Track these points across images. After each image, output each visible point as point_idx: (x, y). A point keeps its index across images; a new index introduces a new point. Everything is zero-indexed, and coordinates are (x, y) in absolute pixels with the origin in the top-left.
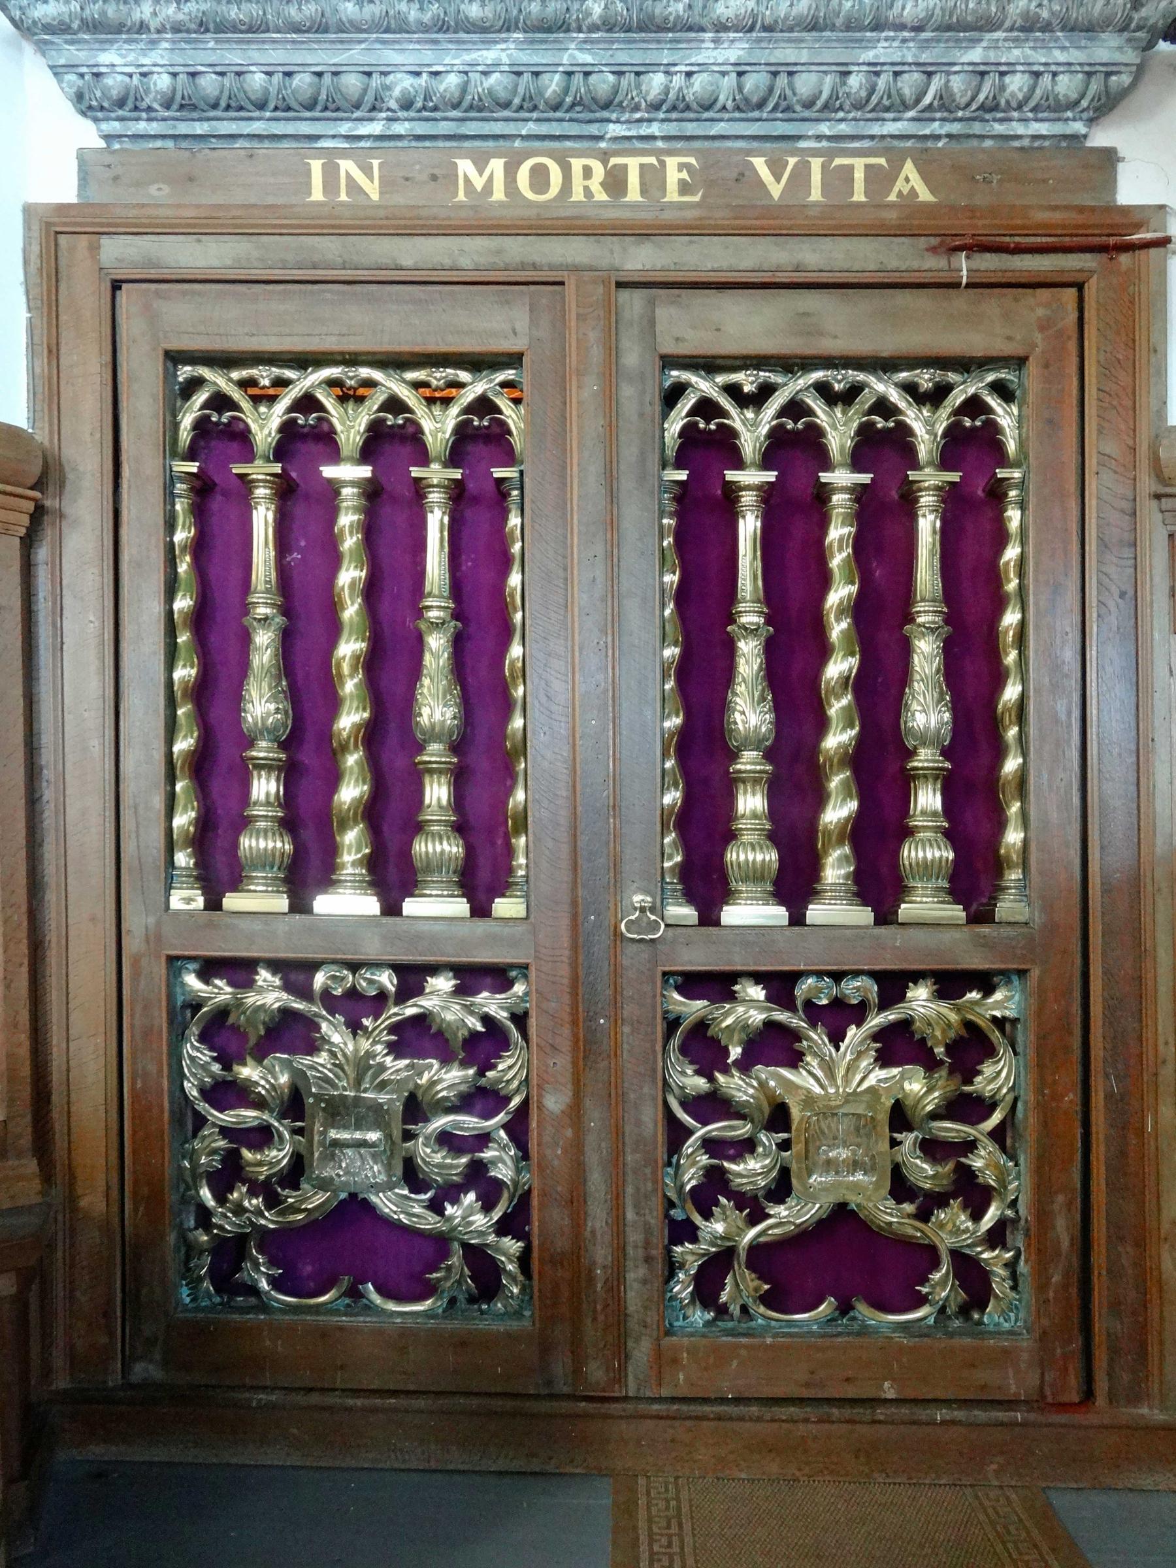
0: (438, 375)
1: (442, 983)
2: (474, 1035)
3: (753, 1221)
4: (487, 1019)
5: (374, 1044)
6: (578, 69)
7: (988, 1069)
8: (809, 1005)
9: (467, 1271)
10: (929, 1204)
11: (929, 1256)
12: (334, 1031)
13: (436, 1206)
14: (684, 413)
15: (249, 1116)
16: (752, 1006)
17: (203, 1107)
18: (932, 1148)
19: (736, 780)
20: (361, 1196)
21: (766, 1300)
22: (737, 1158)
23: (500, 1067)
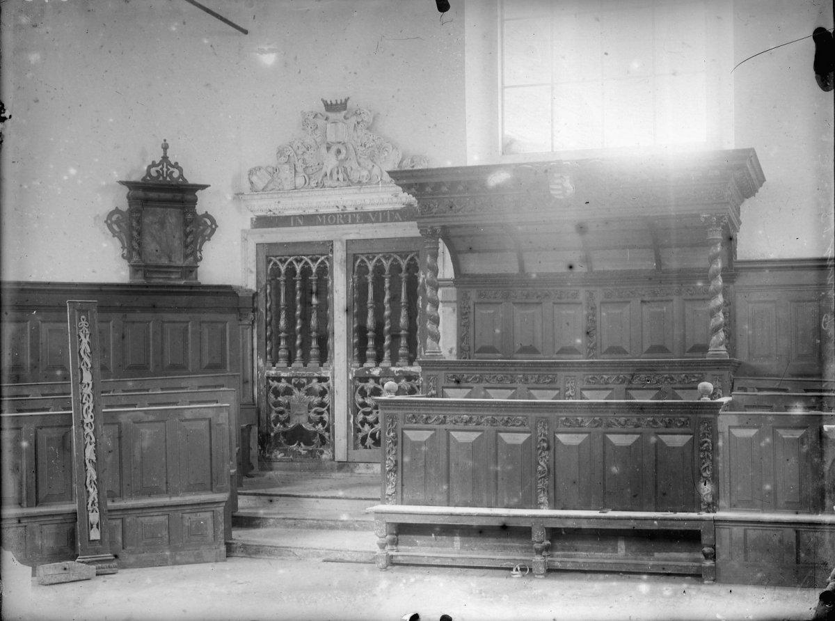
1: (315, 381)
4: (323, 388)
5: (302, 394)
7: (360, 397)
12: (296, 391)
17: (273, 407)
21: (373, 444)
22: (368, 415)
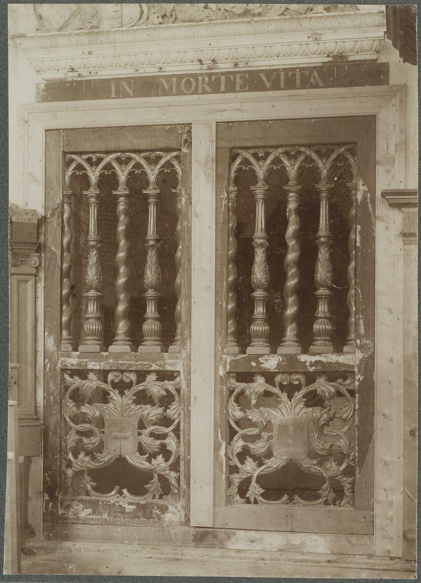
2: (163, 397)
3: (260, 464)
4: (167, 391)
6: (376, 38)
10: (322, 460)
12: (114, 395)
13: (149, 460)
14: (71, 170)
15: (254, 431)
16: (93, 383)
17: (72, 424)
18: (154, 435)
23: (172, 408)
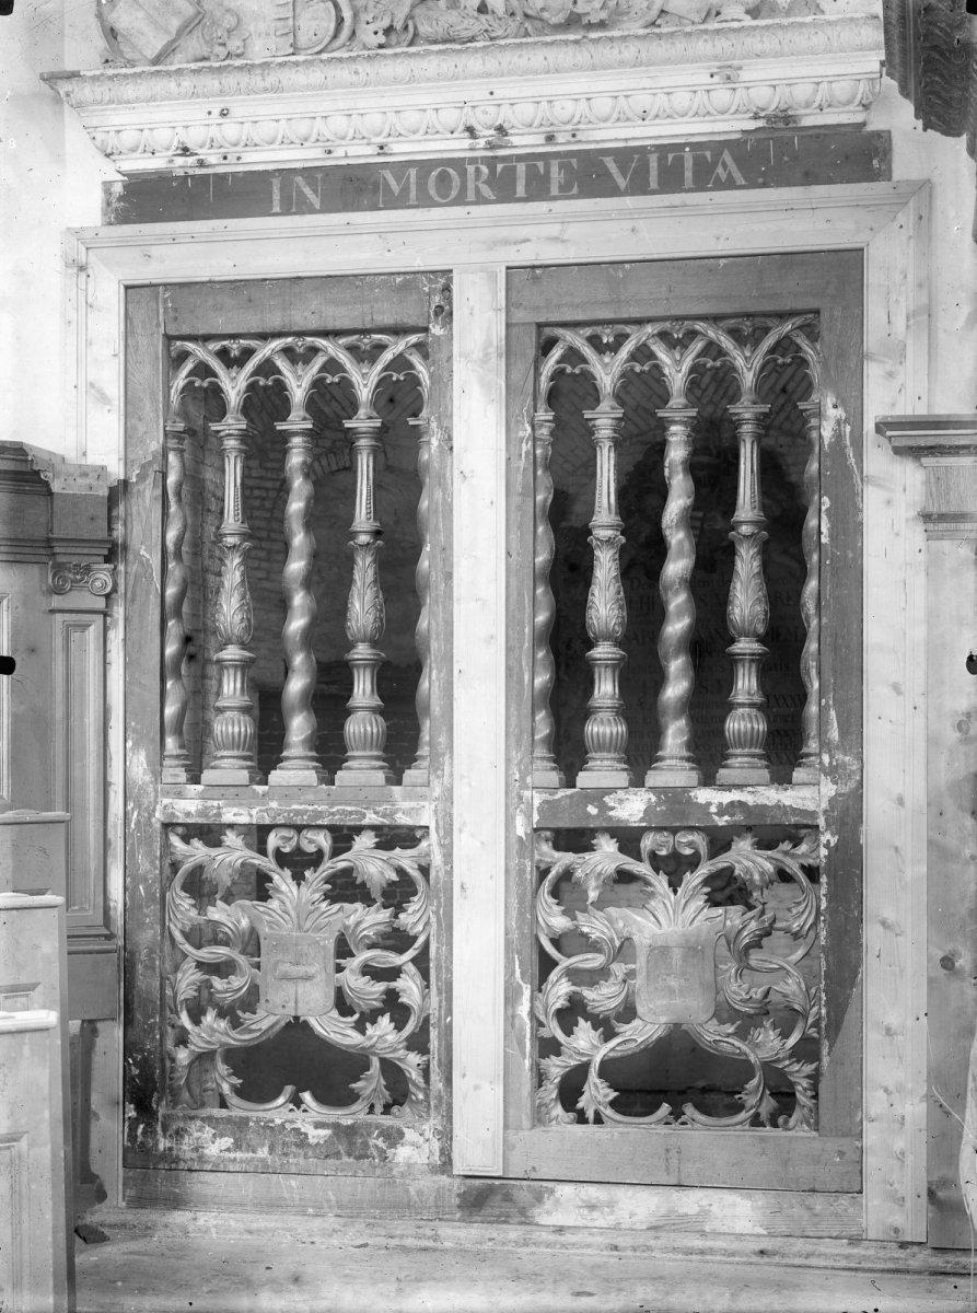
0: (366, 341)
3: (609, 1035)
4: (400, 871)
8: (653, 857)
9: (383, 1082)
11: (744, 1069)
13: (360, 1027)
15: (594, 961)
16: (234, 854)
19: (736, 661)
20: (302, 1019)
22: (592, 984)
23: (410, 911)
